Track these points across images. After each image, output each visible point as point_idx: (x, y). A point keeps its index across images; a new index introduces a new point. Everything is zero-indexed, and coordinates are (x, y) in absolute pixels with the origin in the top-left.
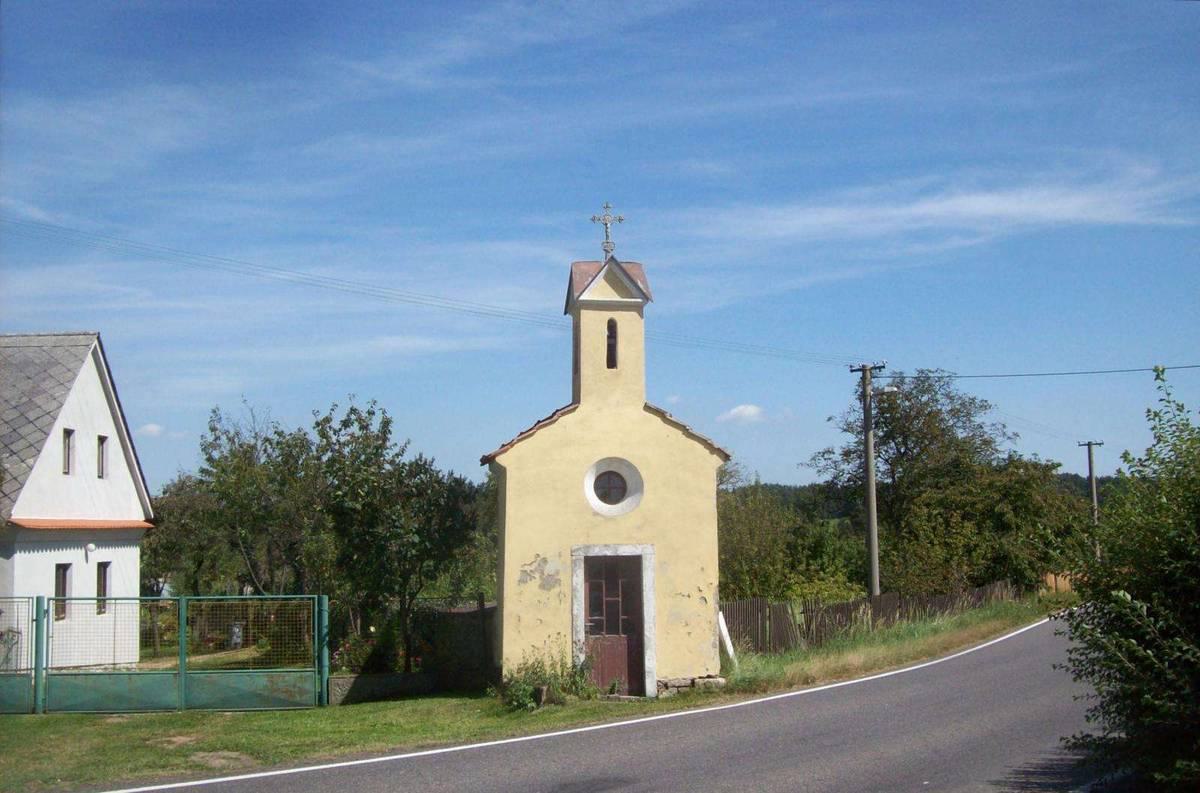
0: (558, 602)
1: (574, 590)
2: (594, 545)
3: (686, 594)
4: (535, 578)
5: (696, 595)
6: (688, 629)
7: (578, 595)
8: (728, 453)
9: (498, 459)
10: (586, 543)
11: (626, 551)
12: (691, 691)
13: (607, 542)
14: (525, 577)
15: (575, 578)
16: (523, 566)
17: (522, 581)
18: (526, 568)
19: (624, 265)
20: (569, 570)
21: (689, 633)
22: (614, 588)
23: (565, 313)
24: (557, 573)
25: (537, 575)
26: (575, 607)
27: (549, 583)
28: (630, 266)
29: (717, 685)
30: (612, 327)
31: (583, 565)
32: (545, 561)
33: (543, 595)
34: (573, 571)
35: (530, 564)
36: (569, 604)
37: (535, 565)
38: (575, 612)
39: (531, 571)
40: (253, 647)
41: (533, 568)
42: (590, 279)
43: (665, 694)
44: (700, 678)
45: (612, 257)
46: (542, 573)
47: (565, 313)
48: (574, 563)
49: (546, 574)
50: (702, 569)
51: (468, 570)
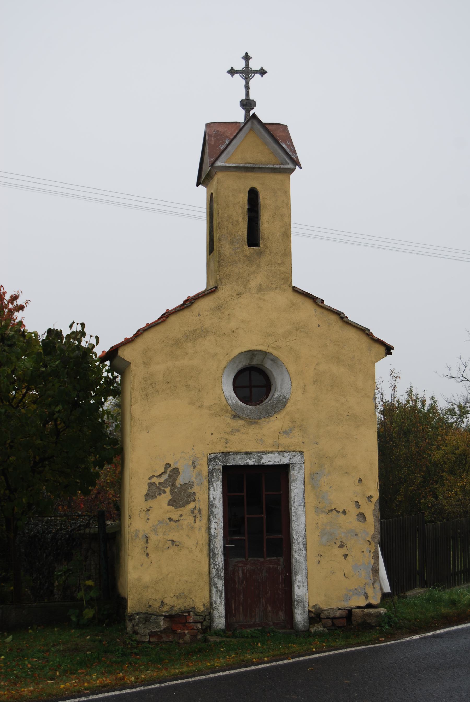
0: (192, 518)
1: (211, 505)
2: (234, 453)
3: (341, 510)
4: (165, 492)
5: (353, 512)
6: (344, 551)
7: (215, 511)
8: (147, 487)
9: (120, 353)
10: (225, 450)
11: (270, 460)
12: (347, 625)
13: (249, 450)
14: (153, 492)
15: (212, 492)
16: (150, 479)
17: (148, 496)
18: (154, 480)
19: (269, 127)
20: (206, 483)
21: (346, 556)
22: (256, 501)
23: (198, 185)
24: (191, 485)
25: (168, 490)
26: (213, 525)
27: (182, 497)
28: (274, 127)
29: (378, 615)
30: (253, 195)
31: (221, 477)
32: (176, 472)
33: (175, 514)
34: (210, 484)
35: (160, 476)
36: (205, 521)
37: (165, 476)
38: (213, 531)
39: (160, 483)
40: (437, 456)
41: (162, 480)
42: (227, 142)
43: (318, 628)
44: (359, 607)
45: (254, 114)
46: (173, 485)
47: (198, 185)
48: (211, 473)
49: (178, 485)
50: (360, 480)
51: (127, 671)
